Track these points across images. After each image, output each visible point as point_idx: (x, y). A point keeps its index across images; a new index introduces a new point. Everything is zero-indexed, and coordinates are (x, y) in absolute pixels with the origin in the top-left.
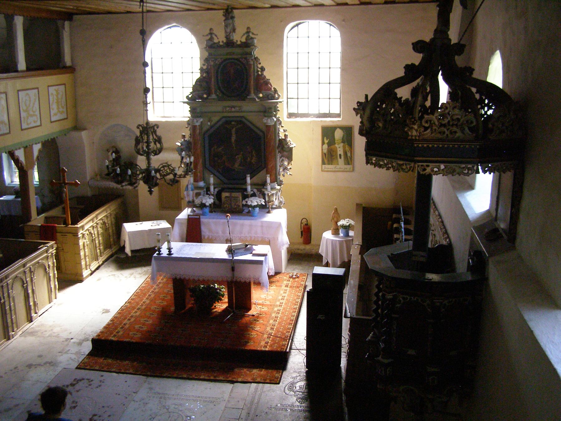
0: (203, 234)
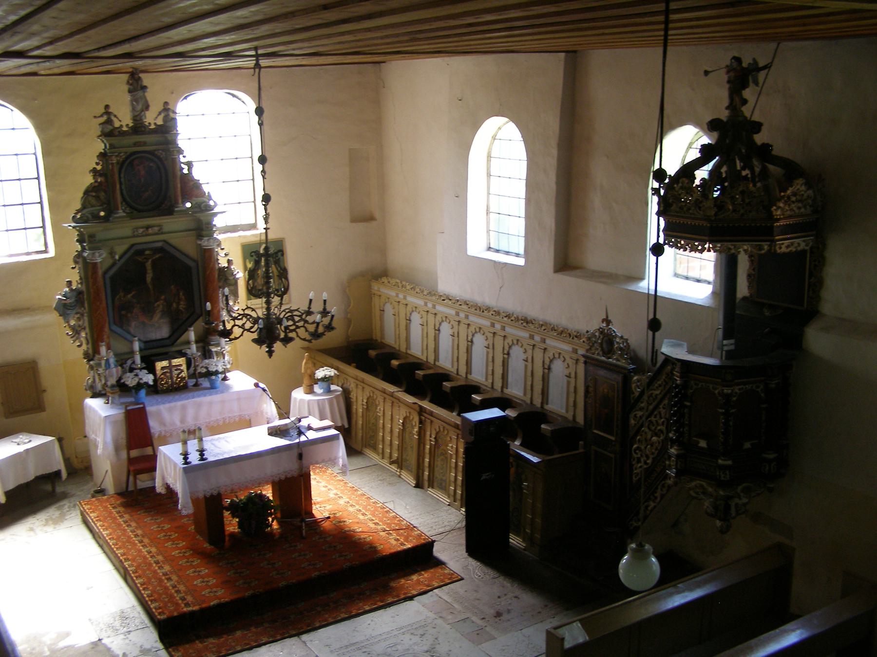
0: (152, 431)
